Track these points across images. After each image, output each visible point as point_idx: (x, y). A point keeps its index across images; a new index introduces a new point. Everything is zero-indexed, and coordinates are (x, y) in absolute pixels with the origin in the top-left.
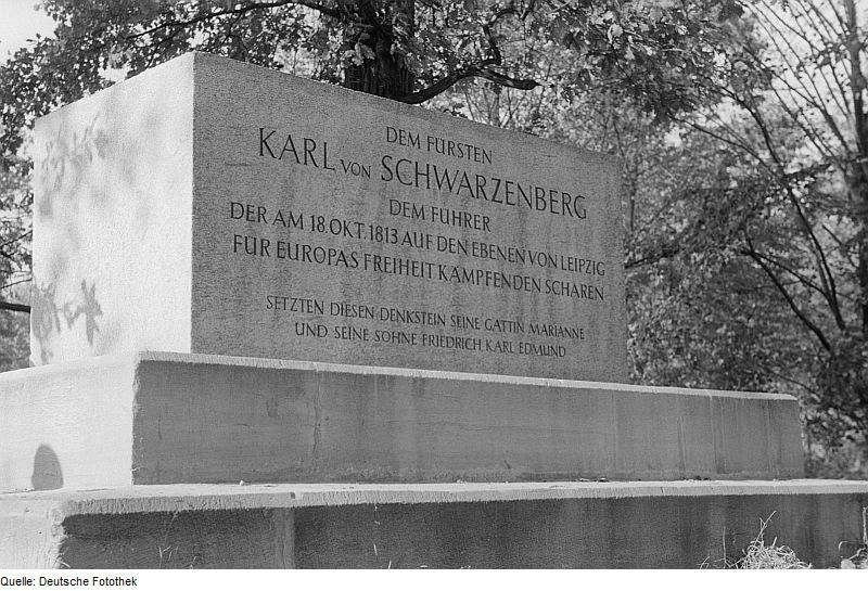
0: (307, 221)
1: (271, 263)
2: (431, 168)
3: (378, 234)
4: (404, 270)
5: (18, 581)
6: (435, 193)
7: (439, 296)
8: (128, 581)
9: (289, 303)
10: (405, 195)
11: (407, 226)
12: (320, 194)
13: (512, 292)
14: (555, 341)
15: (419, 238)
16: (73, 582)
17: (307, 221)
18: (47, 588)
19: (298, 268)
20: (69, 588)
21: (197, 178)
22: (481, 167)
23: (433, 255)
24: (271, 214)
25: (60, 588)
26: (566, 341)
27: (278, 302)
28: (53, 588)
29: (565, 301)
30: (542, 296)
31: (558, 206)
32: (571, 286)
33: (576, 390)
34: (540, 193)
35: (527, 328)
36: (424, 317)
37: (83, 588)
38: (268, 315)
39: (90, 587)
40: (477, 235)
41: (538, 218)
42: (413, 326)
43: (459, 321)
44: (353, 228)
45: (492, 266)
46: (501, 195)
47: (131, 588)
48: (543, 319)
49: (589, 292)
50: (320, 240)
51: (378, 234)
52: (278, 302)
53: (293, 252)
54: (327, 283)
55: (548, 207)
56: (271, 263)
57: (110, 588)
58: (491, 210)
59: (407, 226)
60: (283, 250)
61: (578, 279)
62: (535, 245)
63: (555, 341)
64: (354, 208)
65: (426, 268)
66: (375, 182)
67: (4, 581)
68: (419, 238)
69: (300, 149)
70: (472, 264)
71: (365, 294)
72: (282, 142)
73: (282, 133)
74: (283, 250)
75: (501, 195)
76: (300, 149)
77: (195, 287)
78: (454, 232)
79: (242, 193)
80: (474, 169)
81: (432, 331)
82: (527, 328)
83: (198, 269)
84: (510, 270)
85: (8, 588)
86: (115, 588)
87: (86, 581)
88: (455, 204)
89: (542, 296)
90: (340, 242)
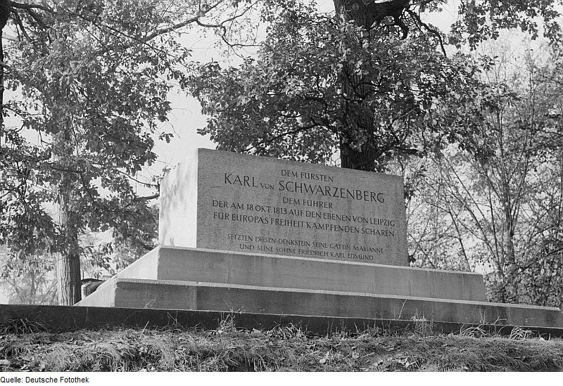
0: (245, 206)
1: (230, 222)
2: (303, 185)
3: (277, 210)
4: (290, 224)
5: (12, 379)
6: (305, 194)
7: (307, 235)
8: (83, 379)
9: (237, 237)
10: (291, 195)
11: (291, 207)
12: (249, 196)
13: (344, 233)
14: (367, 253)
15: (297, 211)
16: (48, 380)
17: (245, 206)
18: (30, 384)
19: (241, 224)
20: (45, 384)
21: (199, 192)
22: (328, 183)
23: (304, 219)
24: (230, 203)
25: (39, 384)
26: (373, 253)
27: (233, 237)
28: (35, 384)
29: (373, 237)
30: (360, 235)
31: (369, 198)
32: (376, 231)
33: (352, 265)
34: (359, 193)
35: (352, 248)
36: (299, 242)
37: (54, 384)
38: (228, 242)
39: (58, 383)
40: (327, 210)
41: (357, 203)
42: (294, 246)
43: (316, 244)
44: (266, 209)
45: (334, 222)
46: (338, 193)
47: (85, 384)
48: (361, 244)
49: (385, 233)
50: (251, 213)
51: (277, 210)
52: (233, 237)
53: (239, 218)
54: (255, 229)
55: (363, 198)
56: (230, 222)
57: (71, 384)
58: (333, 200)
59: (291, 207)
60: (234, 217)
61: (381, 228)
62: (356, 214)
63: (367, 253)
64: (267, 201)
65: (300, 224)
66: (276, 191)
67: (3, 380)
68: (297, 211)
69: (242, 180)
70: (323, 222)
71: (271, 234)
72: (234, 178)
73: (235, 175)
74: (234, 217)
75: (338, 193)
76: (242, 180)
77: (198, 231)
78: (315, 210)
79: (217, 197)
80: (324, 184)
81: (303, 248)
82: (352, 248)
83: (199, 224)
84: (342, 224)
85: (6, 384)
86: (74, 384)
87: (56, 379)
88: (315, 198)
89: (360, 235)
90: (260, 214)
